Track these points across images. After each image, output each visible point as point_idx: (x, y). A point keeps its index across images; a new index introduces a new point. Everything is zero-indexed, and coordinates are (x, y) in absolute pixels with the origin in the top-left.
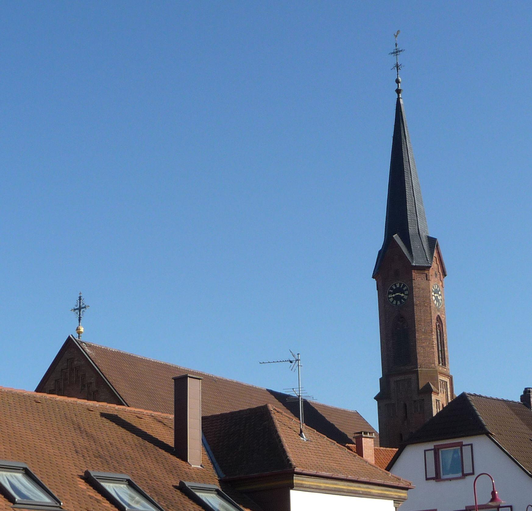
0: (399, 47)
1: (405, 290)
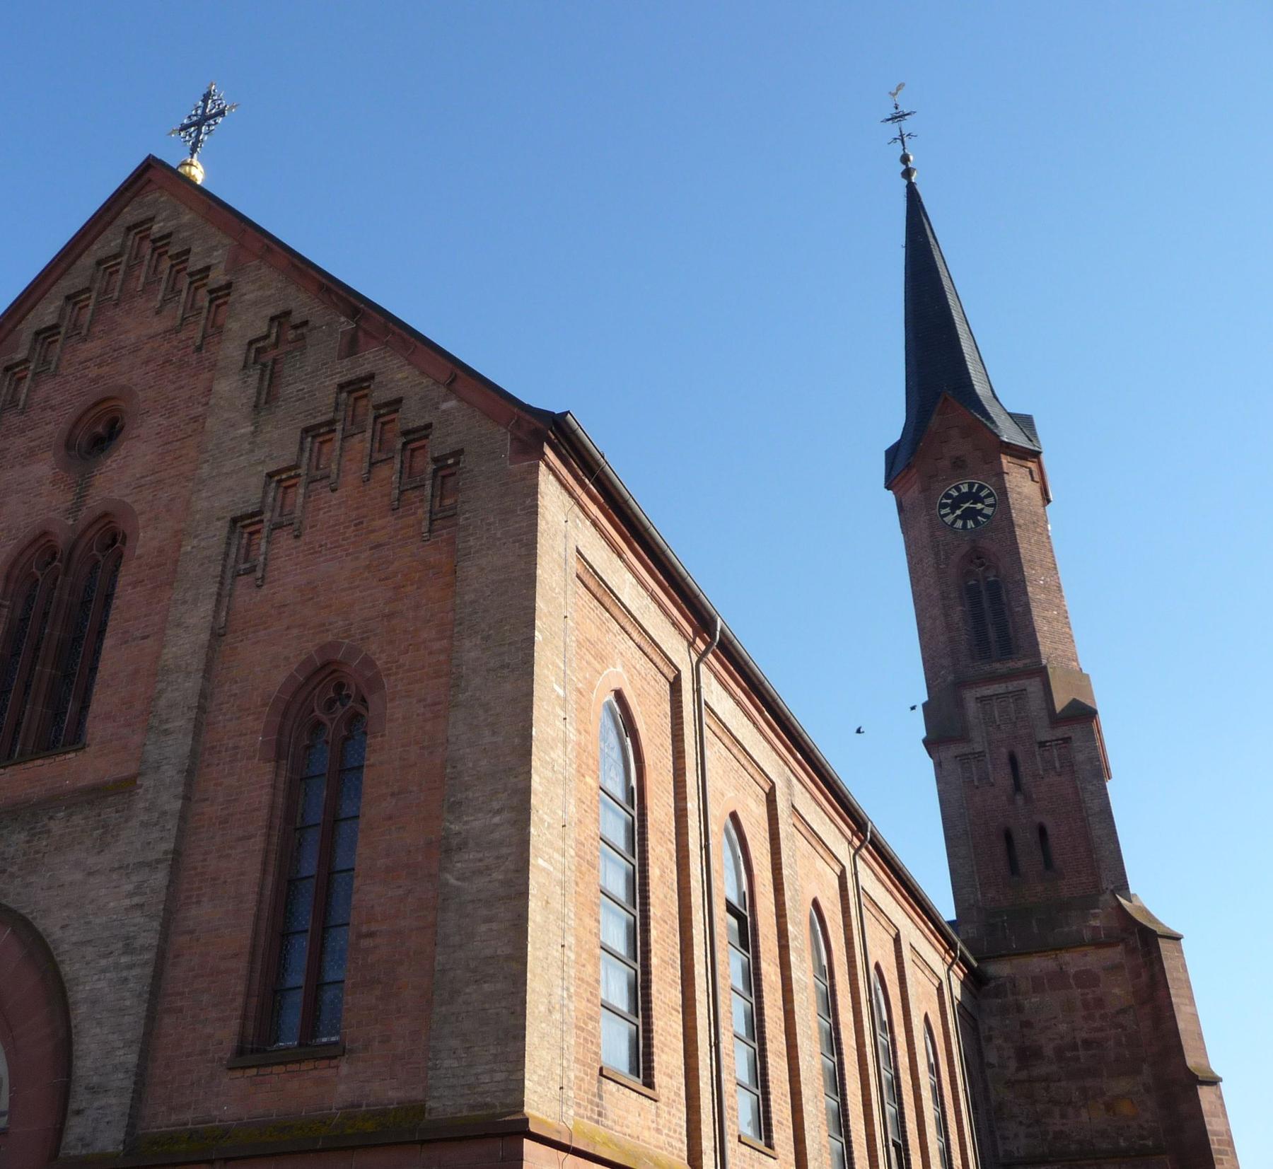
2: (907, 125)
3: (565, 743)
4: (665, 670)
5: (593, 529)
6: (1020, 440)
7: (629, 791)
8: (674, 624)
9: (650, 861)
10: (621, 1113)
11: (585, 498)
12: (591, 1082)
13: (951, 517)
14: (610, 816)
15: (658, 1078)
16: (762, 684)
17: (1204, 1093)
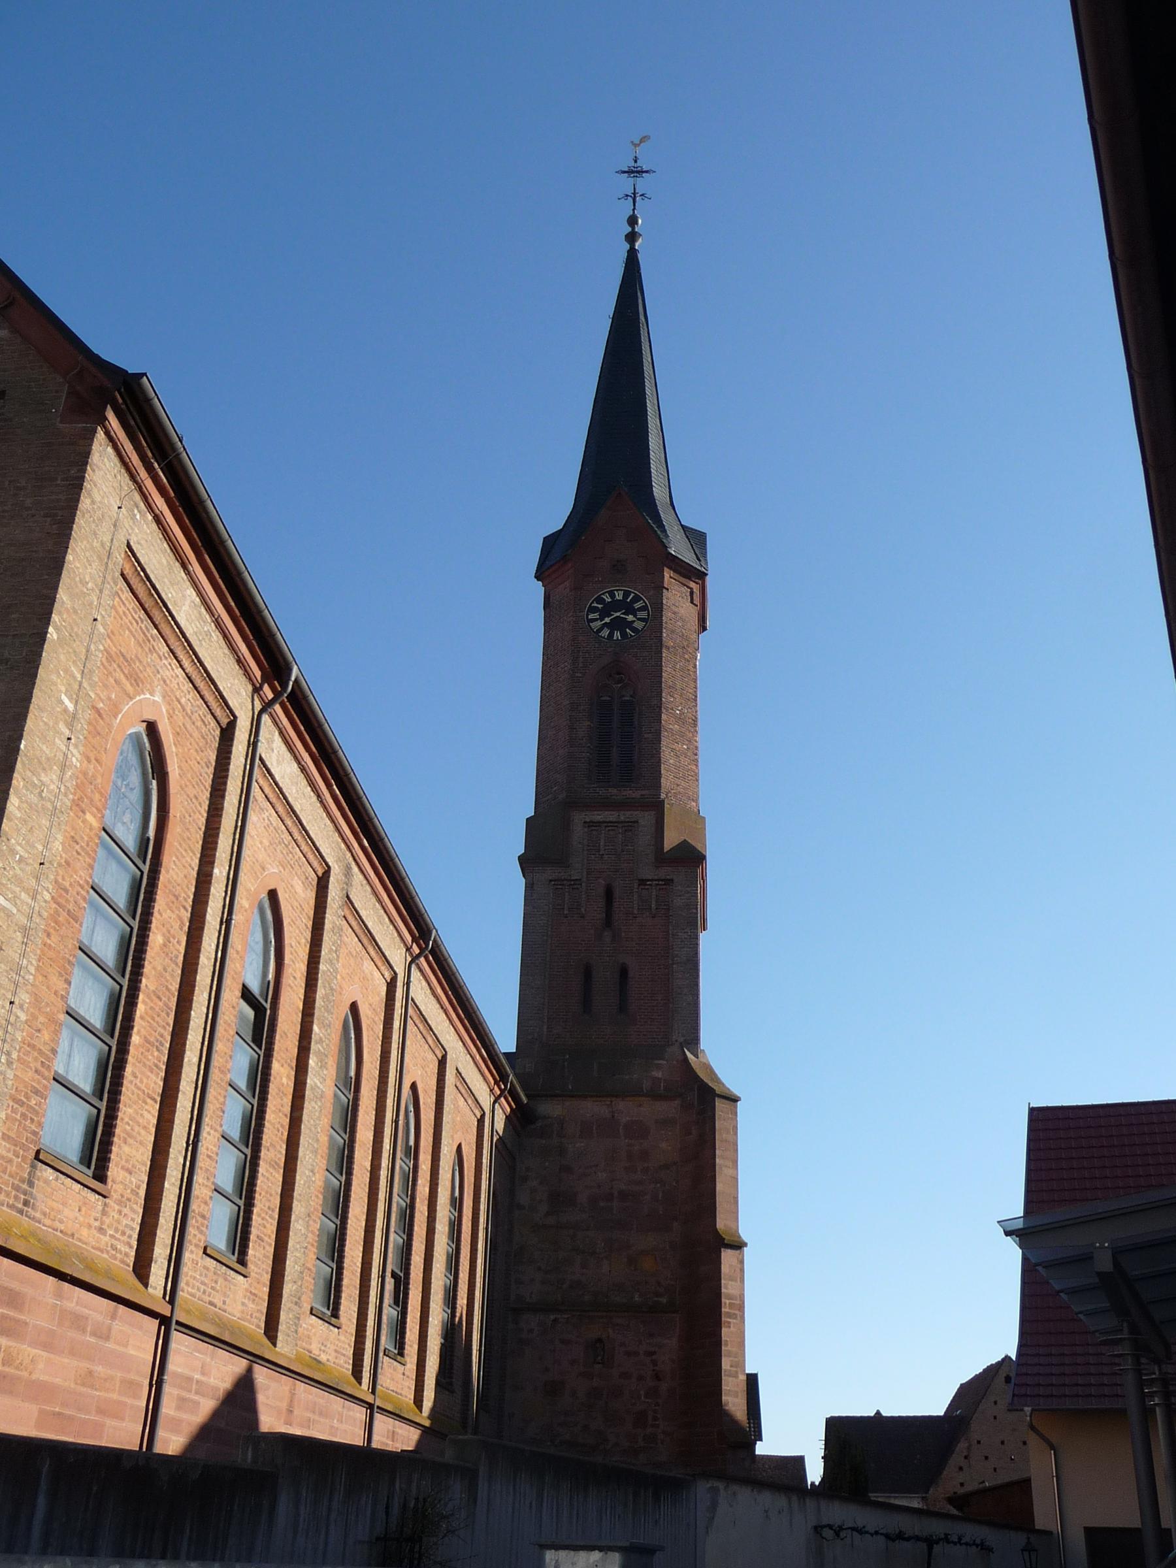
0: (643, 164)
1: (640, 609)
2: (642, 184)
3: (64, 767)
4: (218, 712)
5: (154, 526)
6: (688, 557)
7: (144, 842)
8: (239, 661)
9: (153, 926)
10: (55, 1205)
11: (149, 485)
12: (21, 1165)
13: (599, 623)
14: (114, 866)
15: (113, 1171)
16: (335, 752)
17: (727, 1256)
